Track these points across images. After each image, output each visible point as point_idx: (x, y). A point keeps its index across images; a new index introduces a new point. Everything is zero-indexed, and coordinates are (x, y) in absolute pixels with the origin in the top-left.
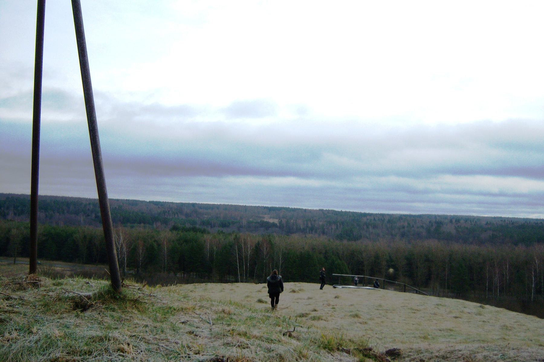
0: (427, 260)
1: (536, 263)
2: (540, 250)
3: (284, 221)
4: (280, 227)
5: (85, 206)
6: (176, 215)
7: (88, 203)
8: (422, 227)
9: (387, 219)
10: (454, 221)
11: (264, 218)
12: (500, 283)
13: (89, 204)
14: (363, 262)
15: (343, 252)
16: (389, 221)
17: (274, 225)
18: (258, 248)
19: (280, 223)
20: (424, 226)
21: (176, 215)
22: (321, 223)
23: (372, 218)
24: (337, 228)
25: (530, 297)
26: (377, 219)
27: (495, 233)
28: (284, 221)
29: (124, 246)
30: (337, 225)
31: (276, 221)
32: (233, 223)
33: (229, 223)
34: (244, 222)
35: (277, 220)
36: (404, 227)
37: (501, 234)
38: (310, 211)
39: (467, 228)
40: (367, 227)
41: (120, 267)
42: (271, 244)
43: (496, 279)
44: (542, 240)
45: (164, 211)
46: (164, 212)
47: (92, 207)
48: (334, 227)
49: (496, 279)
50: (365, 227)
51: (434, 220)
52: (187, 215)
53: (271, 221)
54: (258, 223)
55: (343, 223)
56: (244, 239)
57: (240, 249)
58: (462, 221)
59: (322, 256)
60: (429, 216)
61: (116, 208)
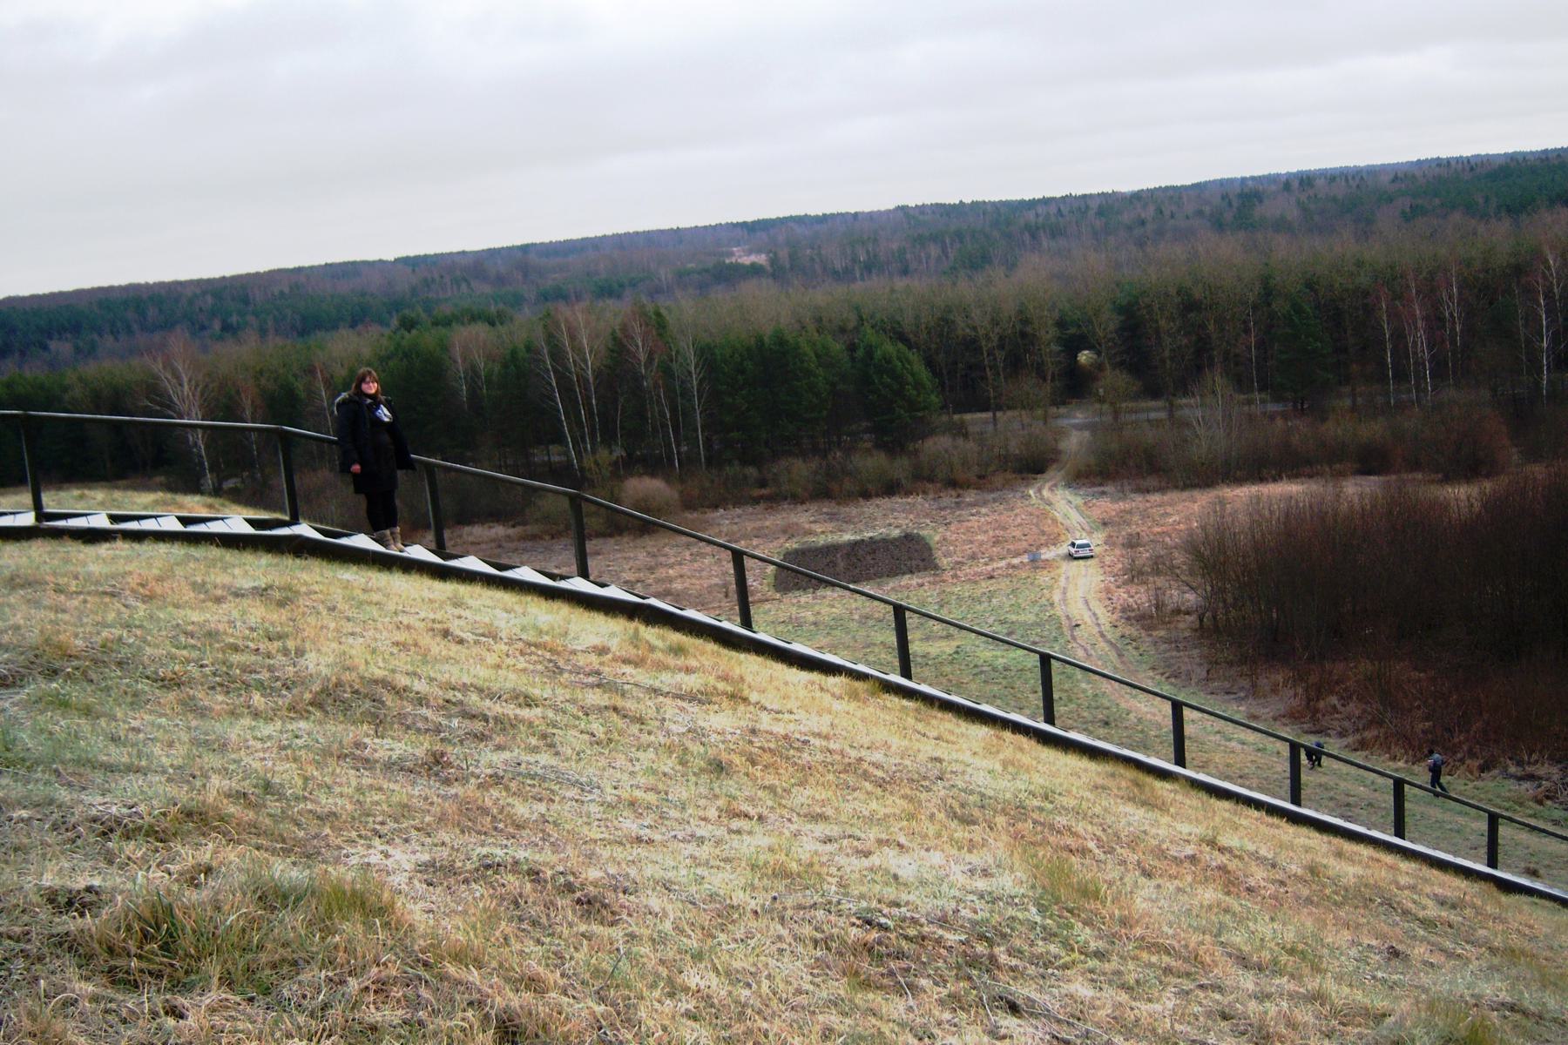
0: (1190, 305)
1: (1549, 268)
2: (1556, 228)
3: (784, 254)
4: (774, 276)
5: (191, 302)
6: (464, 286)
7: (198, 291)
8: (1200, 213)
9: (1094, 205)
10: (1296, 184)
11: (732, 254)
12: (1430, 348)
13: (204, 293)
14: (974, 341)
15: (917, 317)
16: (1101, 212)
17: (755, 270)
18: (619, 348)
19: (773, 262)
20: (1207, 209)
21: (464, 286)
22: (895, 246)
23: (1053, 210)
24: (944, 250)
25: (1538, 384)
26: (1065, 210)
27: (1420, 202)
28: (784, 254)
29: (1094, 604)
30: (944, 242)
31: (761, 259)
32: (633, 284)
33: (621, 286)
34: (665, 275)
35: (763, 256)
36: (1143, 223)
37: (1437, 201)
38: (871, 216)
39: (1334, 199)
40: (1033, 236)
41: (1090, 733)
42: (659, 324)
43: (1419, 339)
44: (1567, 199)
45: (425, 280)
46: (427, 283)
47: (209, 299)
48: (934, 250)
49: (1419, 339)
50: (1027, 237)
51: (1238, 191)
52: (501, 280)
53: (747, 260)
54: (707, 271)
55: (959, 235)
56: (566, 320)
57: (557, 354)
58: (1320, 182)
59: (837, 347)
60: (1222, 183)
61: (282, 293)
